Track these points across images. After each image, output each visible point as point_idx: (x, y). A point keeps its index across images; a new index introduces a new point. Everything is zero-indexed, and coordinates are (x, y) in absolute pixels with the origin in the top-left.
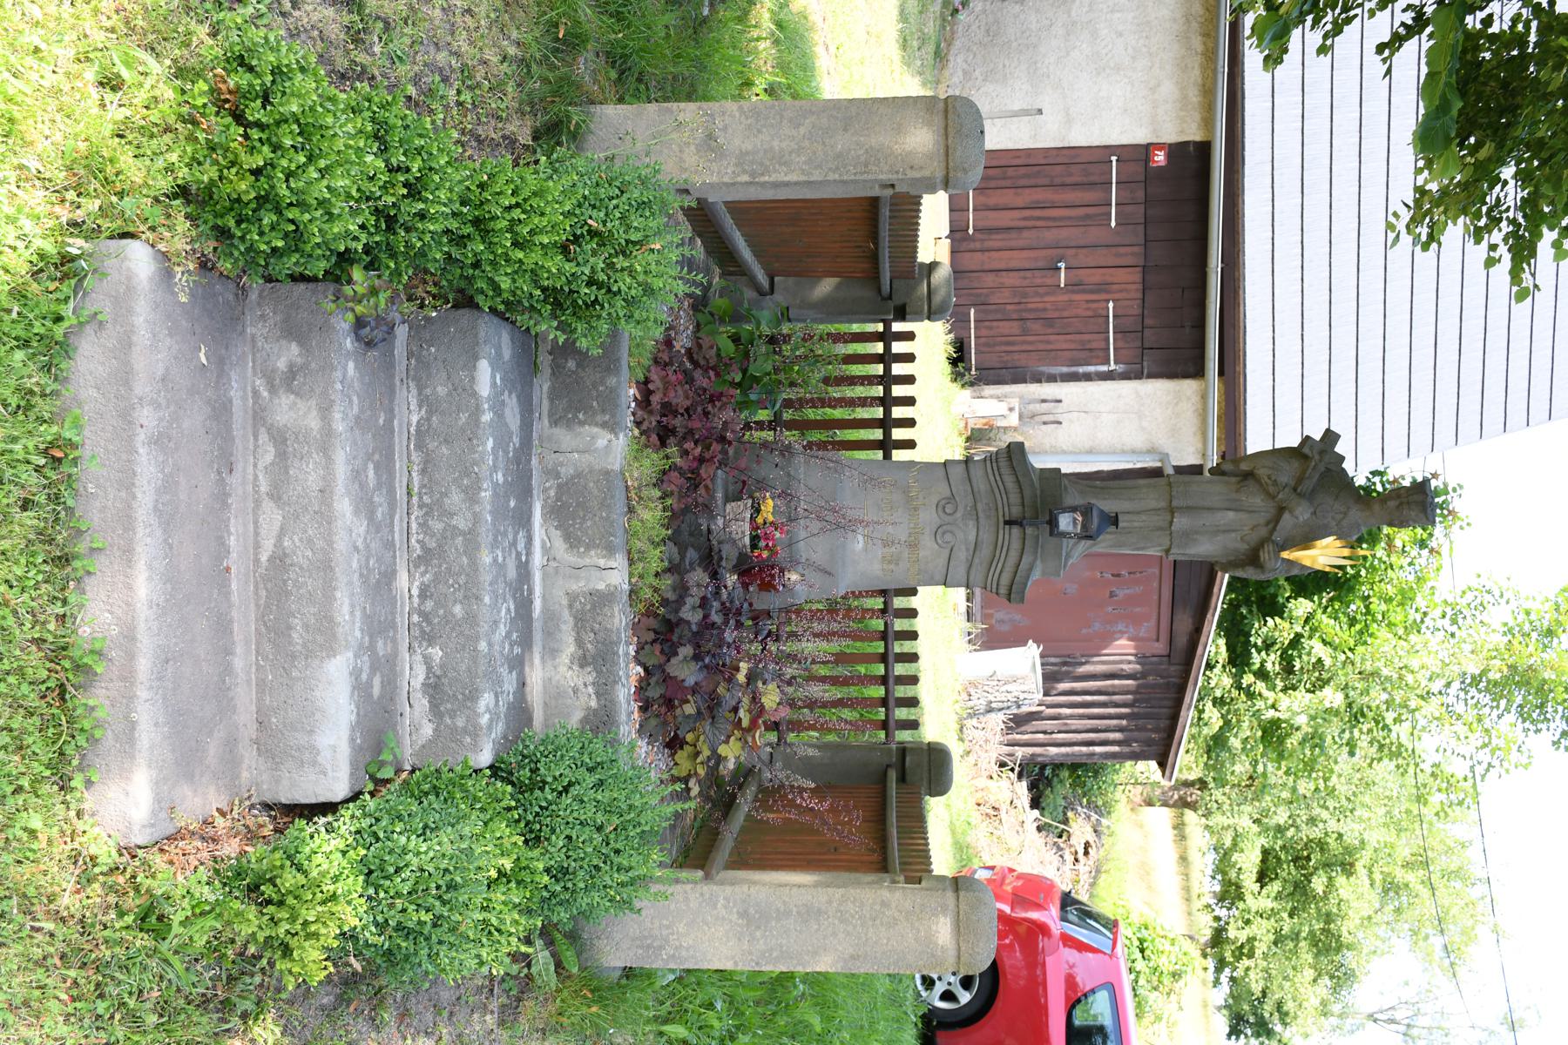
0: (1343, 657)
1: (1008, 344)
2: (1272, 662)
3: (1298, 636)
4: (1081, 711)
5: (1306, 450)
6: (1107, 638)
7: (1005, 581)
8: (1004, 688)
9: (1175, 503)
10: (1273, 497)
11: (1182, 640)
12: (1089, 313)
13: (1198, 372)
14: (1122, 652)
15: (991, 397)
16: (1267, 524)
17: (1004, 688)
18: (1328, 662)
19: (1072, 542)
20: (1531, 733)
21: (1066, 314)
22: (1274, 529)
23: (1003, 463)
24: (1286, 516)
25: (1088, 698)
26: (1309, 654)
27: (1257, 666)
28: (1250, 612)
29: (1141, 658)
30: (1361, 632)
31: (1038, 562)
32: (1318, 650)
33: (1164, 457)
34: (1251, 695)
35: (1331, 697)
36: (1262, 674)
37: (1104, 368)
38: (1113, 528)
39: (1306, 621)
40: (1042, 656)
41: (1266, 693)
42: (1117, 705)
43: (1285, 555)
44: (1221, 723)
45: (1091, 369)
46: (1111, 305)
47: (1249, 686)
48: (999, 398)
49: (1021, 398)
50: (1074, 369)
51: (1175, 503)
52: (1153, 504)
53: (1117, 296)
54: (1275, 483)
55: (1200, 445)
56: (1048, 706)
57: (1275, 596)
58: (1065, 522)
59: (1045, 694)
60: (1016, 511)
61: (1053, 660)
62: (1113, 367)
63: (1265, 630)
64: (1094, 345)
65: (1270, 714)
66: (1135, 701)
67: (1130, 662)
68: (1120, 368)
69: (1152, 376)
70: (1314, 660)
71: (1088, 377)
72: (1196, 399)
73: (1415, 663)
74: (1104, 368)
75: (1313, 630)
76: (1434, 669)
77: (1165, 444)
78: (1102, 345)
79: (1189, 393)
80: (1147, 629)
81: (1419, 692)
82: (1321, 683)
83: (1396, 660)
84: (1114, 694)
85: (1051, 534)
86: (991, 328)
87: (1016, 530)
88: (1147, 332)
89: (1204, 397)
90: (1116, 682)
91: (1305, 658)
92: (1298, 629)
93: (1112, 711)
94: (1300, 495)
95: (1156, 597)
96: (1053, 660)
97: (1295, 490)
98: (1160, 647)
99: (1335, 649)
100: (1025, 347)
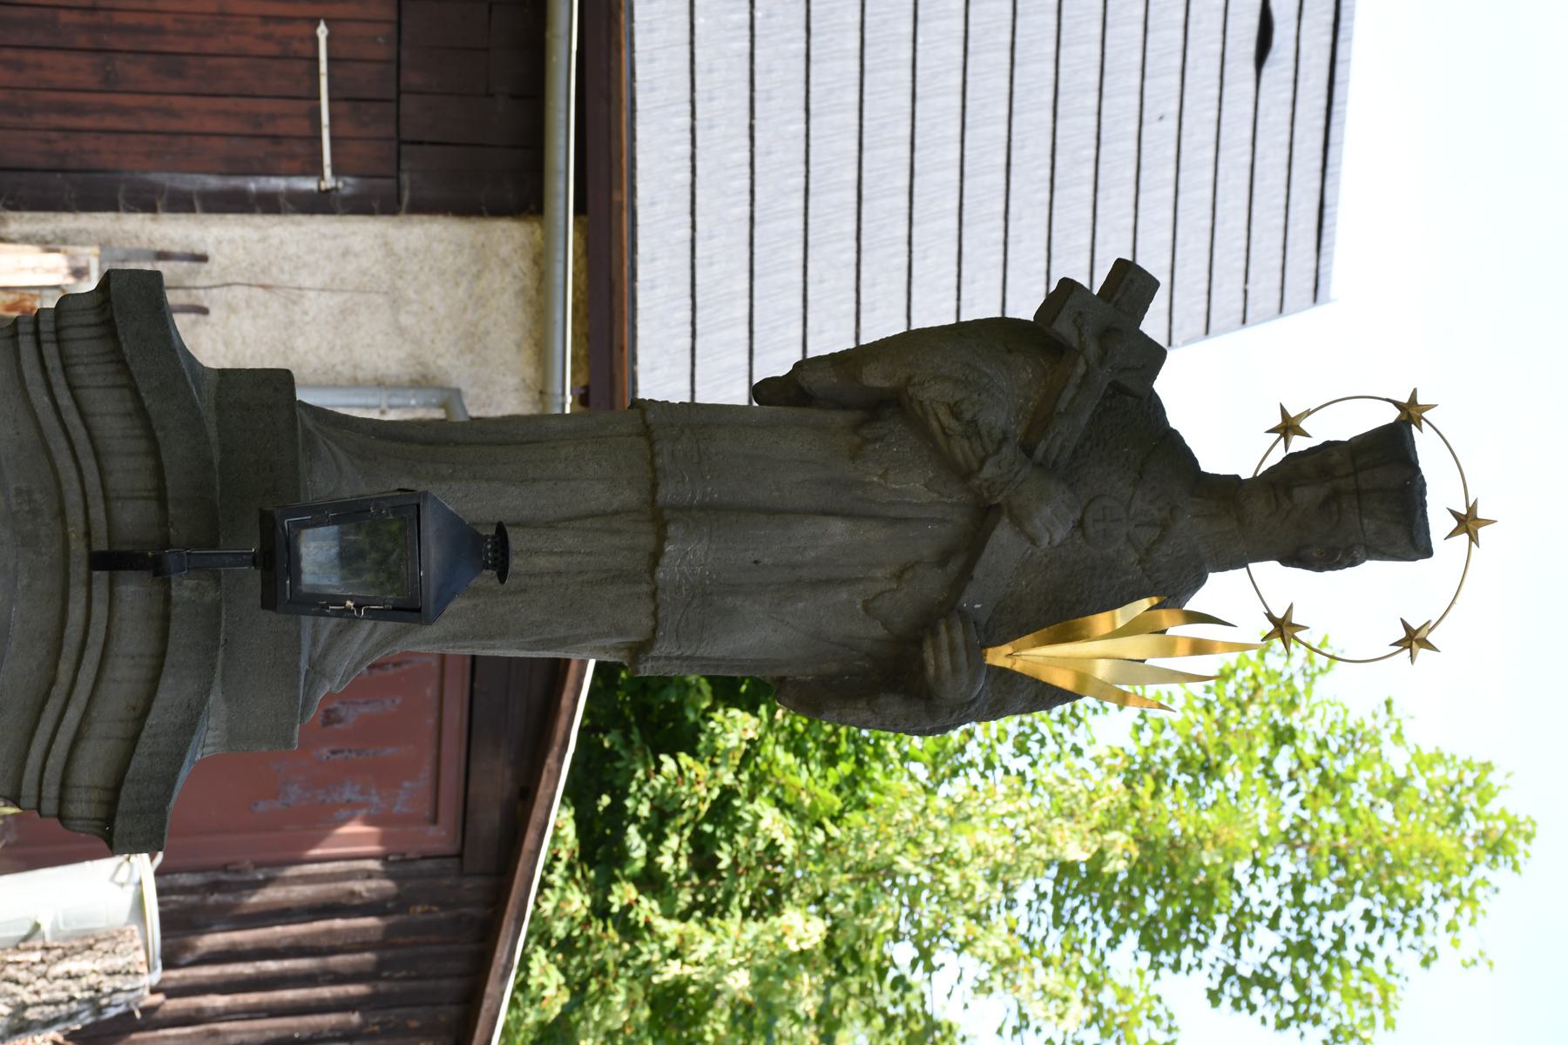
0: (819, 837)
1: (67, 109)
2: (673, 855)
3: (728, 793)
4: (252, 998)
5: (1064, 327)
6: (321, 821)
7: (92, 769)
8: (60, 969)
9: (666, 493)
10: (964, 475)
11: (489, 818)
12: (270, 48)
13: (527, 201)
14: (352, 850)
15: (26, 239)
16: (943, 560)
17: (60, 969)
18: (789, 848)
19: (328, 625)
20: (1165, 972)
21: (211, 45)
22: (966, 574)
23: (85, 347)
24: (1003, 534)
25: (271, 966)
26: (751, 833)
27: (640, 864)
28: (628, 744)
29: (393, 863)
30: (852, 781)
31: (215, 699)
32: (774, 824)
33: (451, 397)
34: (630, 930)
35: (801, 927)
36: (651, 881)
37: (309, 184)
38: (488, 578)
39: (747, 757)
40: (159, 873)
41: (663, 925)
42: (338, 978)
43: (999, 657)
44: (565, 998)
45: (278, 184)
46: (322, 32)
47: (627, 908)
48: (47, 245)
49: (105, 245)
50: (235, 182)
51: (666, 493)
52: (598, 496)
53: (338, 11)
54: (973, 429)
55: (530, 372)
56: (172, 993)
57: (680, 706)
58: (317, 554)
59: (168, 964)
60: (134, 519)
61: (184, 879)
62: (329, 182)
63: (658, 782)
64: (282, 127)
65: (672, 970)
66: (381, 965)
67: (369, 875)
68: (346, 185)
69: (423, 207)
70: (761, 845)
71: (269, 204)
72: (520, 264)
73: (963, 846)
74: (309, 184)
75: (758, 781)
76: (999, 856)
77: (453, 367)
78: (303, 127)
79: (505, 250)
80: (410, 794)
81: (969, 906)
82: (767, 903)
83: (928, 840)
84: (333, 951)
85: (270, 600)
86: (19, 67)
87: (133, 590)
88: (409, 105)
89: (541, 261)
90: (338, 923)
91: (741, 840)
92: (728, 778)
93: (326, 992)
94: (1046, 468)
95: (431, 721)
96: (184, 879)
97: (1028, 449)
98: (439, 837)
99: (801, 819)
100: (110, 122)
